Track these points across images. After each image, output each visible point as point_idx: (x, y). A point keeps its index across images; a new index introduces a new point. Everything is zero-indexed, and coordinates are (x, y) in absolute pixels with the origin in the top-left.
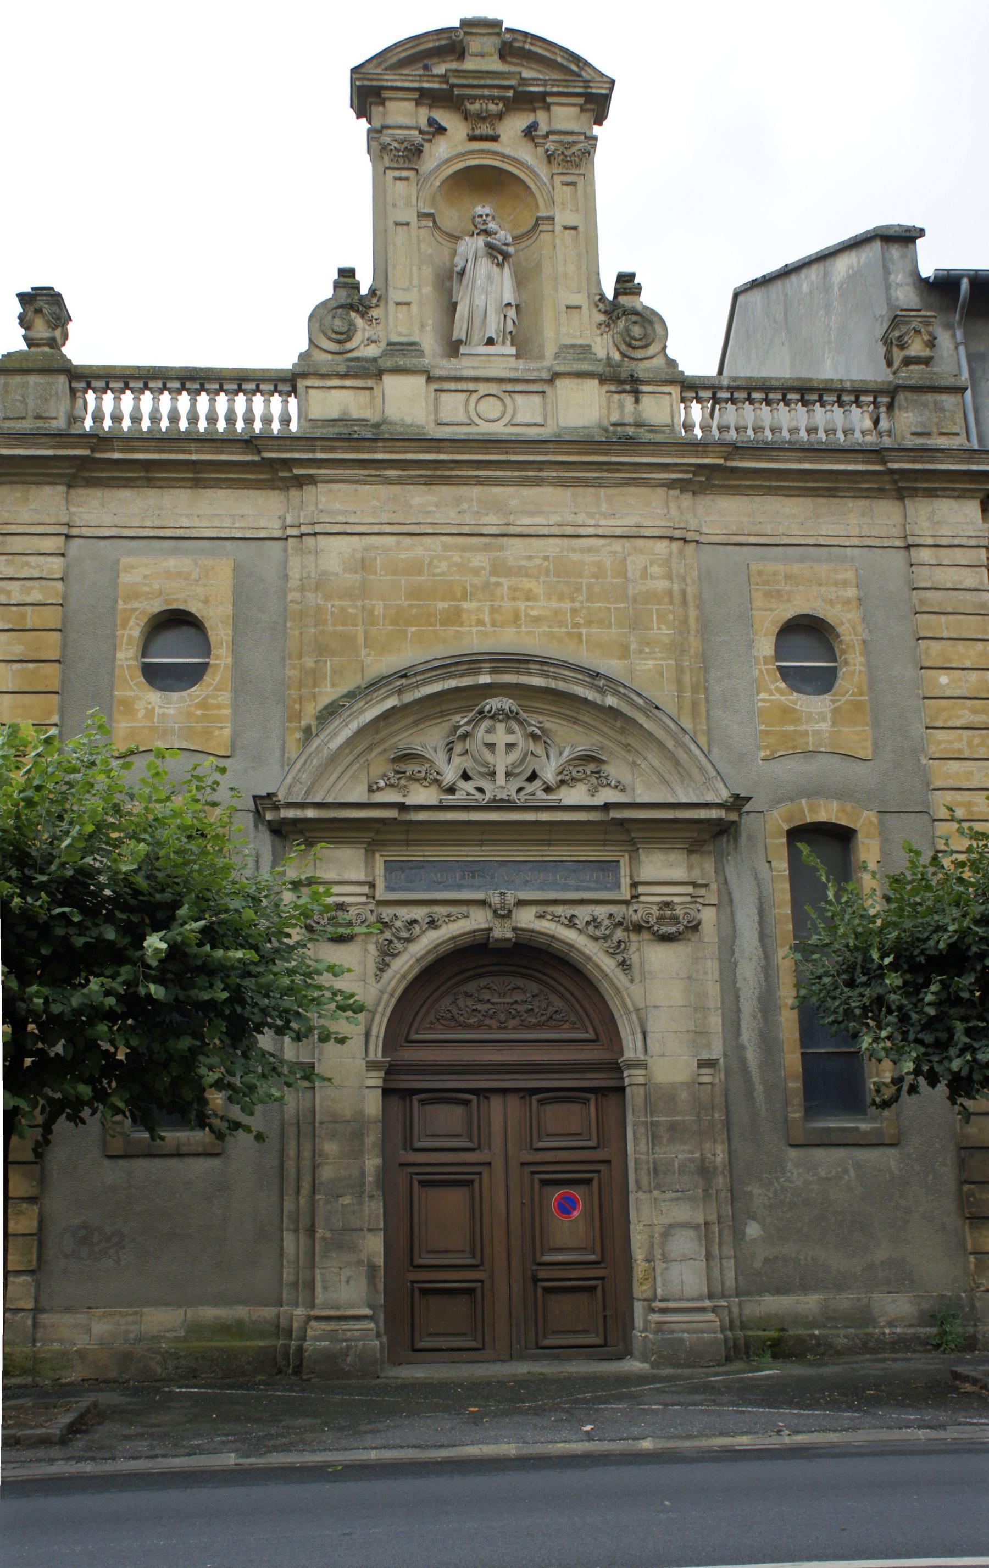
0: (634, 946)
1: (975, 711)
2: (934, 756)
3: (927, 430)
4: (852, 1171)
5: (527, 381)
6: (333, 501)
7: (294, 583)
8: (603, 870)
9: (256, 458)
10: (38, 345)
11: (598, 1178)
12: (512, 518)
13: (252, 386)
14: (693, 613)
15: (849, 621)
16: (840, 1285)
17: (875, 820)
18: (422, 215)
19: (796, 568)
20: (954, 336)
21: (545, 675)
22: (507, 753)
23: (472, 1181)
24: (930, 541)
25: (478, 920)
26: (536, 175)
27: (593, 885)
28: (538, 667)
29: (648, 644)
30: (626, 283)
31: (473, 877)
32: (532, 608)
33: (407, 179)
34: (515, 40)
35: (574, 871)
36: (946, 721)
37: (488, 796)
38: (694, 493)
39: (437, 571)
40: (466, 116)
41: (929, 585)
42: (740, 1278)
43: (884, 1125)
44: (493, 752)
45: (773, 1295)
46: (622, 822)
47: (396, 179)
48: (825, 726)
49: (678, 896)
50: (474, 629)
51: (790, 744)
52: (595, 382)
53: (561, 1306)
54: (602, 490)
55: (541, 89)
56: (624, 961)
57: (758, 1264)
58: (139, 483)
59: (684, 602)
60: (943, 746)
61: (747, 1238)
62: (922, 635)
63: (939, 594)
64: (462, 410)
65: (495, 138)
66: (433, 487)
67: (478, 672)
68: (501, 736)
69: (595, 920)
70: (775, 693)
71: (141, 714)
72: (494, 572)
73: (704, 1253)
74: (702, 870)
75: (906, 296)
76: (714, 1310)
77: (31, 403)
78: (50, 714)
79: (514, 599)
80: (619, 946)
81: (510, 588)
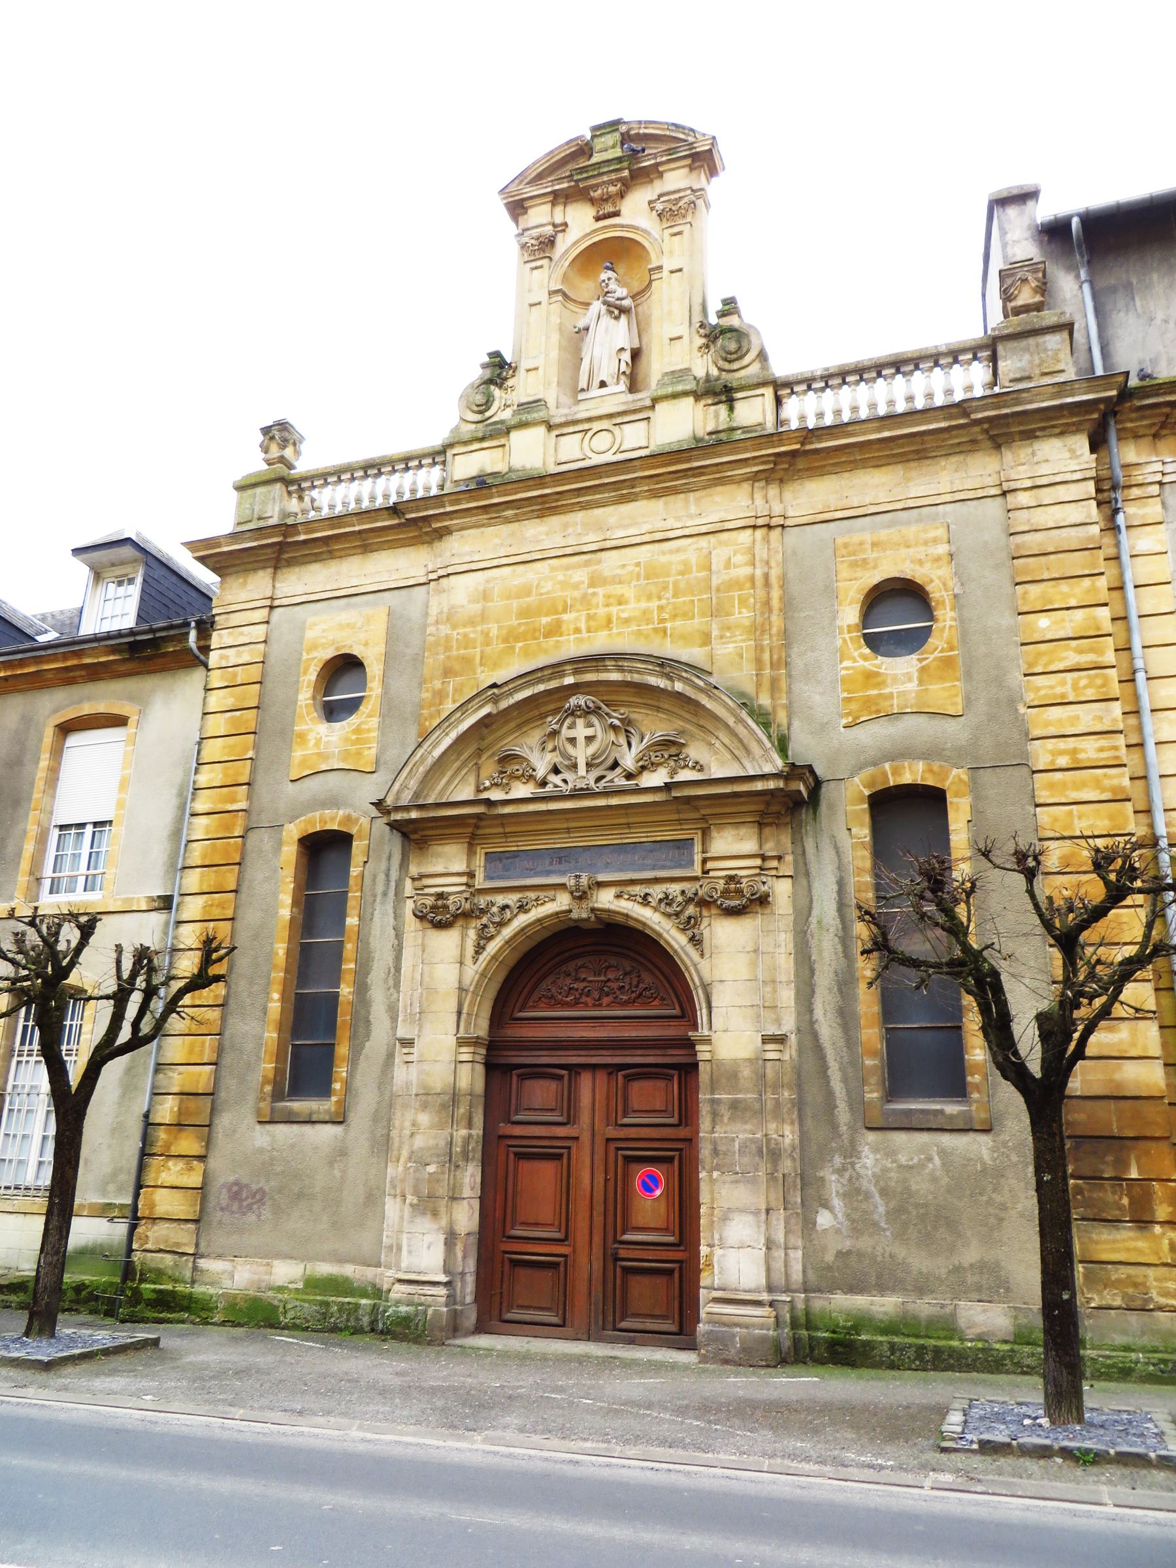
0: (705, 922)
1: (1080, 651)
2: (1032, 704)
3: (1027, 374)
4: (937, 1161)
5: (634, 411)
6: (469, 544)
7: (431, 619)
8: (678, 848)
9: (403, 521)
10: (273, 464)
11: (679, 1159)
12: (609, 533)
13: (416, 463)
14: (776, 594)
15: (939, 578)
16: (922, 1289)
17: (965, 777)
18: (552, 293)
19: (883, 534)
20: (1078, 276)
21: (621, 669)
22: (587, 745)
23: (561, 1155)
24: (1028, 483)
25: (562, 901)
26: (649, 233)
27: (668, 863)
28: (613, 663)
29: (729, 628)
30: (730, 307)
31: (560, 863)
32: (623, 611)
33: (541, 267)
34: (630, 130)
35: (651, 851)
36: (1047, 665)
37: (570, 786)
38: (781, 481)
39: (544, 591)
40: (592, 201)
41: (1027, 528)
42: (810, 1272)
43: (974, 1108)
44: (575, 746)
45: (845, 1293)
46: (688, 800)
47: (533, 269)
48: (912, 686)
49: (744, 869)
50: (572, 637)
51: (873, 709)
52: (691, 400)
53: (641, 1287)
54: (691, 494)
55: (652, 162)
56: (694, 936)
57: (830, 1257)
58: (324, 556)
59: (767, 584)
60: (1043, 692)
61: (818, 1228)
62: (1018, 580)
63: (1039, 536)
64: (577, 447)
65: (617, 214)
66: (545, 519)
67: (562, 675)
68: (581, 731)
69: (667, 897)
70: (861, 658)
71: (312, 743)
72: (592, 584)
73: (763, 1240)
74: (778, 842)
75: (1026, 249)
76: (771, 1304)
77: (256, 508)
78: (247, 750)
79: (607, 605)
80: (688, 922)
81: (604, 596)
